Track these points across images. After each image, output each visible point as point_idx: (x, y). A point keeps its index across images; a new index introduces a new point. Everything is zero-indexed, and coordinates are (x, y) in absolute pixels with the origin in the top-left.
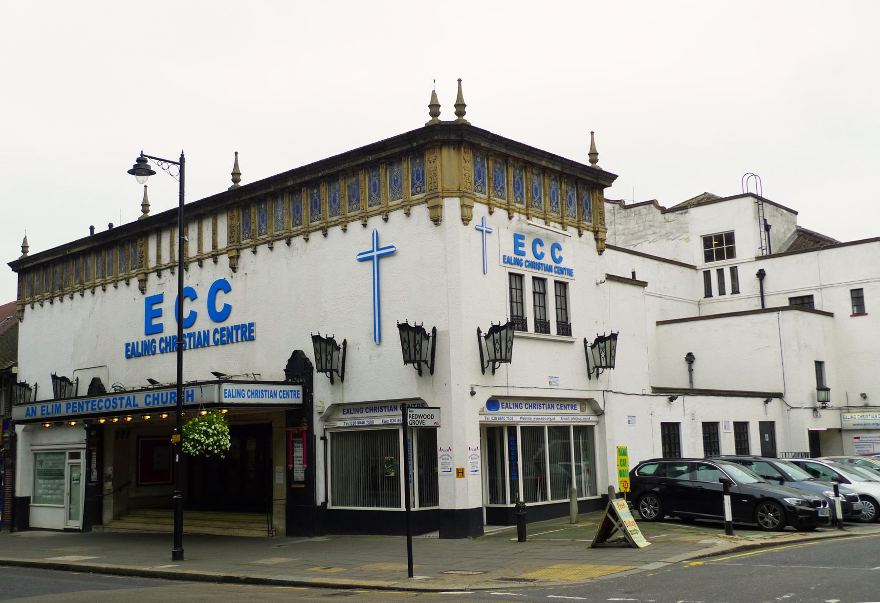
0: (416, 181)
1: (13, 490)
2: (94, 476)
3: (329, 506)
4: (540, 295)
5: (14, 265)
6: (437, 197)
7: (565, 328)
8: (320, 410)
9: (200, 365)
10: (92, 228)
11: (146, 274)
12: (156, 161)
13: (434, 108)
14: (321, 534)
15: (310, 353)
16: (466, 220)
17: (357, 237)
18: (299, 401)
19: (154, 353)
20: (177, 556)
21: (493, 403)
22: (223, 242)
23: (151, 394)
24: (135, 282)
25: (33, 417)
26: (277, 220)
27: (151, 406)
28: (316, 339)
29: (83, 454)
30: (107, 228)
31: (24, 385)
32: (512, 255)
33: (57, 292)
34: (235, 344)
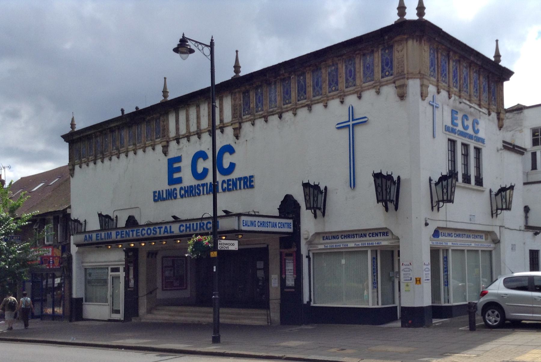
0: (385, 67)
1: (71, 294)
2: (132, 283)
3: (312, 304)
4: (466, 155)
5: (66, 137)
6: (404, 78)
7: (479, 182)
8: (306, 236)
9: (227, 201)
10: (122, 111)
11: (168, 142)
12: (194, 43)
13: (402, 9)
14: (307, 323)
15: (299, 197)
16: (423, 96)
17: (337, 111)
18: (291, 230)
19: (175, 198)
20: (216, 340)
21: (436, 233)
22: (228, 116)
23: (184, 224)
24: (159, 148)
25: (90, 242)
26: (271, 101)
27: (184, 233)
28: (306, 186)
29: (122, 269)
30: (135, 110)
31: (77, 221)
32: (449, 124)
33: (99, 156)
34: (239, 191)
